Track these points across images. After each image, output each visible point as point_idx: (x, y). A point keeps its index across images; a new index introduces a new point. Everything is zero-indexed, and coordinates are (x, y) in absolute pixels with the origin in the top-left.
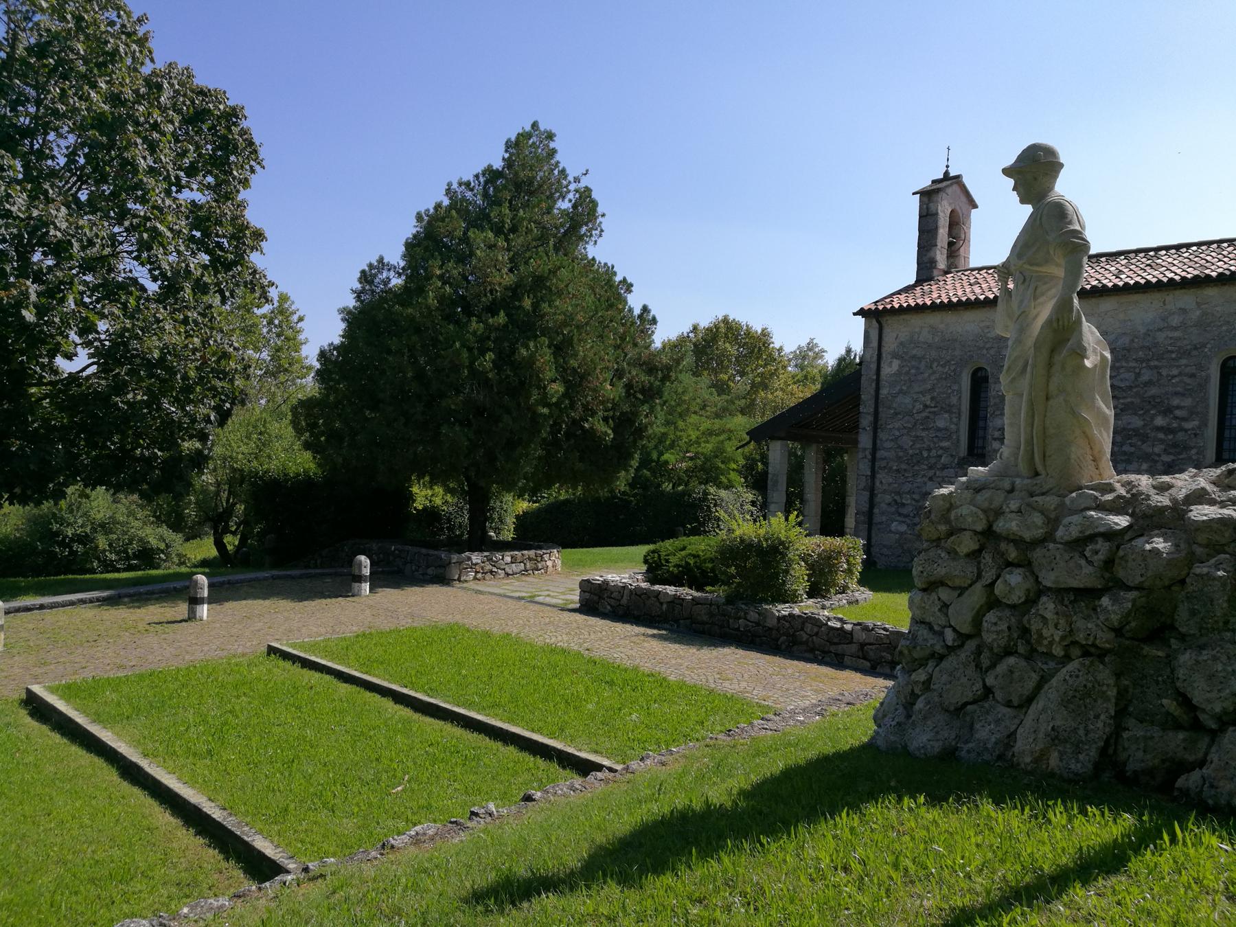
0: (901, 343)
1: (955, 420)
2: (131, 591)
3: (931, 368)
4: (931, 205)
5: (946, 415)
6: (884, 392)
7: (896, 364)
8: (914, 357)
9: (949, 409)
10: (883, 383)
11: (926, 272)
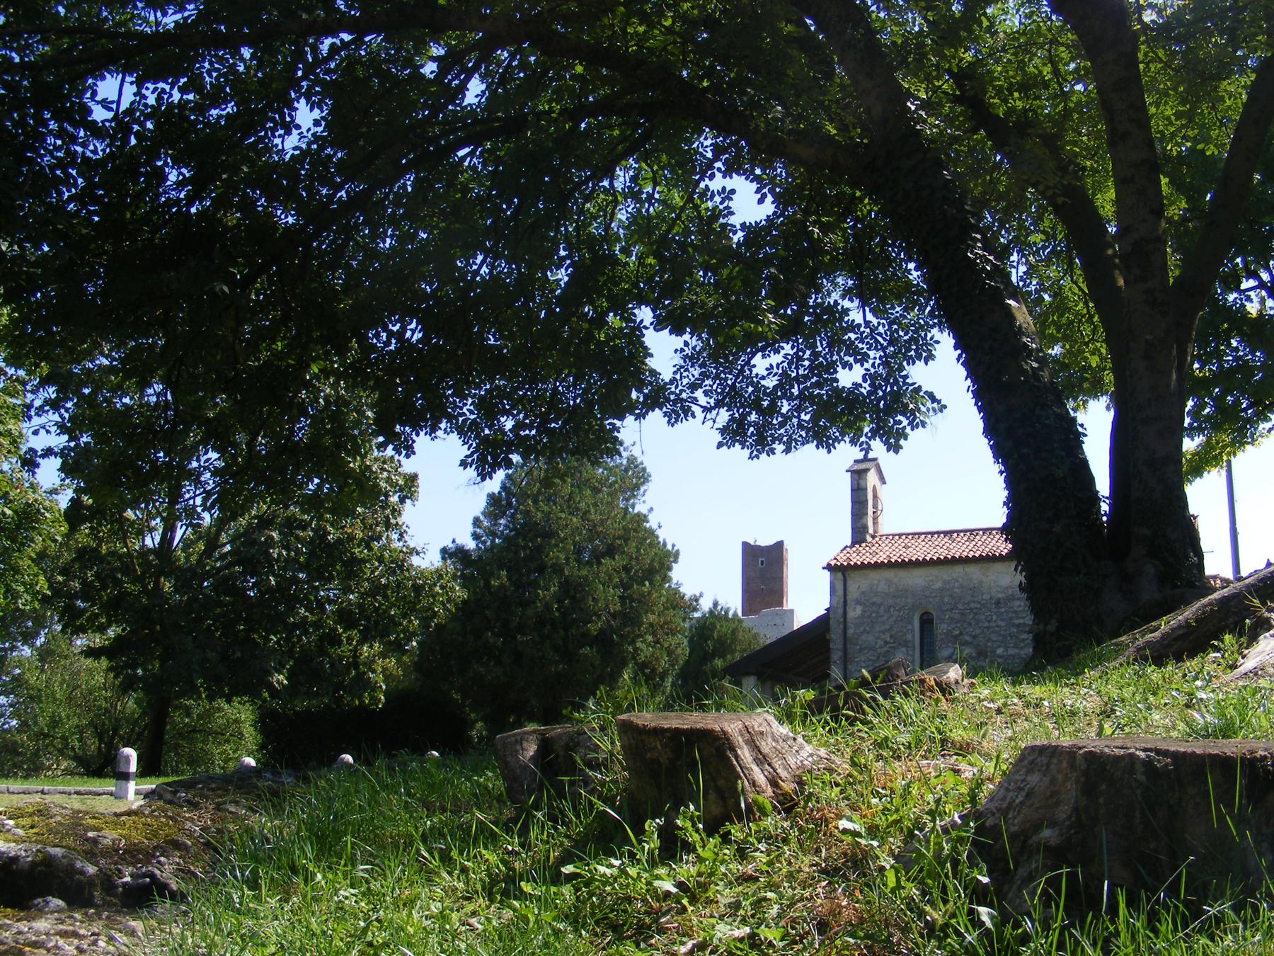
0: (863, 593)
1: (911, 652)
2: (873, 704)
3: (889, 612)
4: (861, 482)
5: (904, 649)
6: (850, 632)
7: (859, 610)
8: (874, 604)
9: (906, 644)
10: (849, 625)
11: (859, 533)
